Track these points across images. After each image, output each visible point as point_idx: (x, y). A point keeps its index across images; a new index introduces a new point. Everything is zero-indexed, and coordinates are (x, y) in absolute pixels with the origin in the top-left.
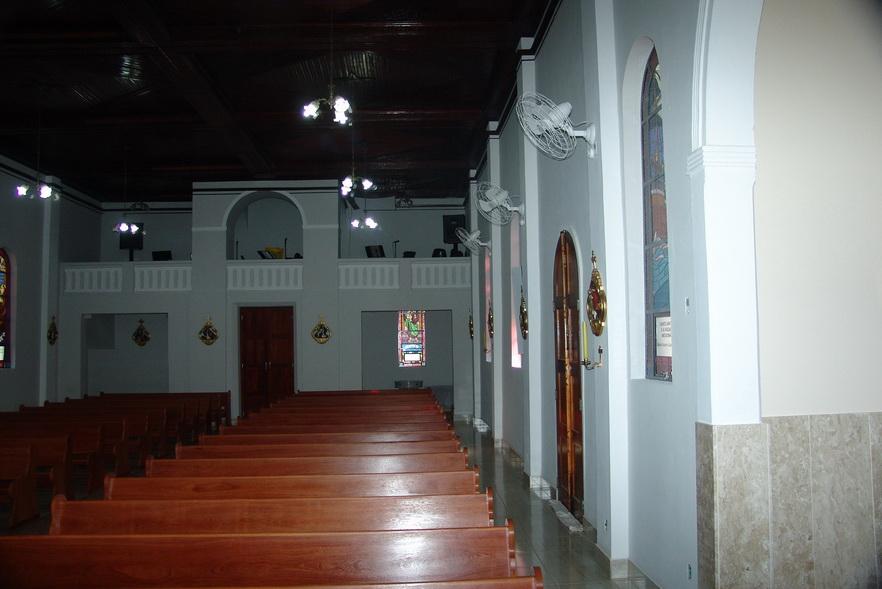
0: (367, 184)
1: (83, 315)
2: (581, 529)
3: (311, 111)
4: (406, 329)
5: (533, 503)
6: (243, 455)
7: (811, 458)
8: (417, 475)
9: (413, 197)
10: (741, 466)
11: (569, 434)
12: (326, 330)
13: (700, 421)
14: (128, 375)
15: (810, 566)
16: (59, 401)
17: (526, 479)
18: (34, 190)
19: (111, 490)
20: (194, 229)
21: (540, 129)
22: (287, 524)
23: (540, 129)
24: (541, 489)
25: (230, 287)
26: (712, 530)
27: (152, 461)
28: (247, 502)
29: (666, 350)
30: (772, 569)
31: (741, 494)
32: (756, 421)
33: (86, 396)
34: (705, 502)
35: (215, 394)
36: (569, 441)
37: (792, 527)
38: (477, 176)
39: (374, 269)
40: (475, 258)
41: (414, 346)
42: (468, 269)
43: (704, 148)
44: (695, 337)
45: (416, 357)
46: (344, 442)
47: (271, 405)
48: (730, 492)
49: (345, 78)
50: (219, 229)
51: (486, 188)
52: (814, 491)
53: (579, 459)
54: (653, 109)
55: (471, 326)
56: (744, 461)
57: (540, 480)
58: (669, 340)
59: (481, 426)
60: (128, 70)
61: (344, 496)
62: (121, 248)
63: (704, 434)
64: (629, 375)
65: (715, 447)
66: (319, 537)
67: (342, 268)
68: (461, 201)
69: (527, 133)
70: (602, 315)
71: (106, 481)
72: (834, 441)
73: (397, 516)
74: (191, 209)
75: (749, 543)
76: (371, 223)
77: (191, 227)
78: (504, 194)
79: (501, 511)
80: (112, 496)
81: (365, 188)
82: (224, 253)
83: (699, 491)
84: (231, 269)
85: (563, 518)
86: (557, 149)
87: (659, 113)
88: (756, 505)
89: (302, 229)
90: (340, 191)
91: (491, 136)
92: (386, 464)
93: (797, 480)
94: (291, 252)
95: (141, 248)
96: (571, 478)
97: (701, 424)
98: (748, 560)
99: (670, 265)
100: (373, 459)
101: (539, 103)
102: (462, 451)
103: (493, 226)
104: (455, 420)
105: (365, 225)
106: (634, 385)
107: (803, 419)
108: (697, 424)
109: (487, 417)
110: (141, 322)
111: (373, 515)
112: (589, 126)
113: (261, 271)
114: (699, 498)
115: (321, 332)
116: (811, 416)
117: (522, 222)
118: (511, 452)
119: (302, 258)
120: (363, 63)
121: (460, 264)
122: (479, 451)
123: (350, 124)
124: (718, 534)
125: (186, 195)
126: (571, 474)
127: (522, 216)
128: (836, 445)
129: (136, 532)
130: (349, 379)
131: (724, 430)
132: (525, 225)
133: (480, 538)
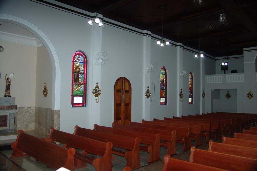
1: (212, 90)
18: (199, 56)
19: (224, 140)
20: (244, 63)
27: (236, 133)
33: (213, 112)
35: (253, 114)
60: (222, 18)
71: (223, 138)
74: (243, 57)
80: (225, 143)
95: (228, 70)
110: (228, 91)
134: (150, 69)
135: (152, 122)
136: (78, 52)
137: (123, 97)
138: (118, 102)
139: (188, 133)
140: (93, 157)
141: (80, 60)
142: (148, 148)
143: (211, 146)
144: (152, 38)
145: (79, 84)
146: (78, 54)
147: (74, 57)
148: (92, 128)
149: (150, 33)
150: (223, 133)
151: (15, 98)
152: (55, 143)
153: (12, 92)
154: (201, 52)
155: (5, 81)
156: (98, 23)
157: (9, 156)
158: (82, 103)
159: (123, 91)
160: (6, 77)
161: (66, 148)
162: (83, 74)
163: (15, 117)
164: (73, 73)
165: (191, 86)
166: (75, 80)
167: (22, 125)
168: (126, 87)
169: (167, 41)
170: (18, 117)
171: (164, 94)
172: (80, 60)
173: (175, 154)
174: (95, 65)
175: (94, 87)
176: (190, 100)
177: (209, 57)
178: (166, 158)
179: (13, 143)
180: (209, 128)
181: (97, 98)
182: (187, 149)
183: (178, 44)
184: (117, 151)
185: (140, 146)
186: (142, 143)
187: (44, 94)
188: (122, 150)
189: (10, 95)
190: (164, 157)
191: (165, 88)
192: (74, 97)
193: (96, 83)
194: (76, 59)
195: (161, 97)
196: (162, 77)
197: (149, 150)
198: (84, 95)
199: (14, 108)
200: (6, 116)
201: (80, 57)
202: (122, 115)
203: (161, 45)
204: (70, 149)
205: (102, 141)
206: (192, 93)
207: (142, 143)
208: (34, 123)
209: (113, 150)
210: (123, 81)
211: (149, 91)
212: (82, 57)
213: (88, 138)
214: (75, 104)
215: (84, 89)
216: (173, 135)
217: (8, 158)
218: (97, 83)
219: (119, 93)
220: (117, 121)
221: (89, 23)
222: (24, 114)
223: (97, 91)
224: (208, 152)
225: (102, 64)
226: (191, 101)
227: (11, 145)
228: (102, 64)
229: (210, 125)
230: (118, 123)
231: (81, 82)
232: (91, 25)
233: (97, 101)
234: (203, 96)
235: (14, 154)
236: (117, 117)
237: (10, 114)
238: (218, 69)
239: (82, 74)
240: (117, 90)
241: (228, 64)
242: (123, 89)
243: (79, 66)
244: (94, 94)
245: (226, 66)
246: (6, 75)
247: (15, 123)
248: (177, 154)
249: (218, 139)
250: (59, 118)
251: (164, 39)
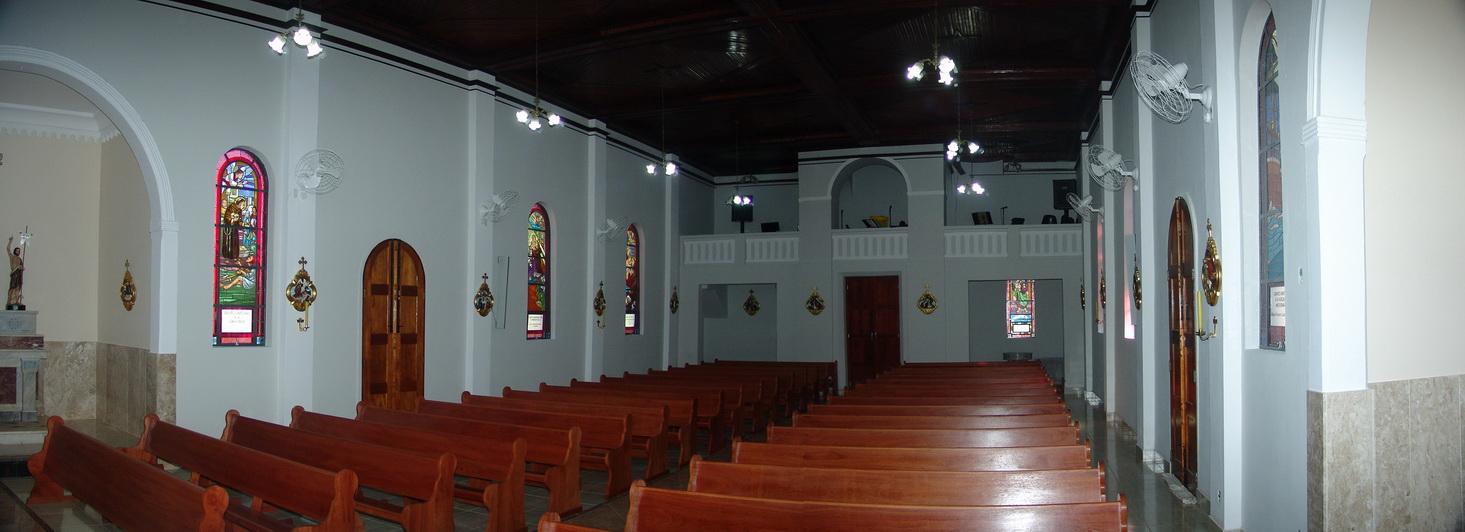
0: (974, 148)
1: (700, 286)
2: (1194, 502)
3: (915, 72)
4: (1015, 299)
5: (1146, 477)
6: (851, 425)
7: (1410, 420)
8: (1026, 450)
9: (1021, 161)
10: (1348, 431)
11: (1183, 406)
12: (931, 300)
13: (1311, 389)
14: (737, 342)
15: (1408, 519)
16: (679, 366)
17: (1139, 453)
18: (661, 168)
19: (737, 453)
21: (1155, 90)
22: (894, 496)
23: (1155, 90)
24: (1154, 462)
25: (836, 257)
26: (1321, 496)
28: (854, 472)
29: (1279, 320)
30: (1374, 525)
31: (1349, 458)
32: (1363, 387)
33: (703, 362)
34: (1315, 468)
36: (1183, 413)
37: (1393, 485)
38: (1089, 137)
39: (981, 236)
40: (1087, 225)
41: (1022, 316)
42: (1079, 239)
43: (1319, 119)
44: (1308, 307)
45: (1026, 328)
46: (947, 415)
47: (877, 376)
48: (1338, 458)
49: (950, 36)
50: (824, 198)
51: (1099, 151)
52: (1413, 450)
53: (1193, 431)
54: (1270, 76)
55: (1083, 296)
56: (1350, 426)
57: (1153, 453)
58: (1282, 310)
59: (1092, 400)
60: (736, 45)
61: (950, 470)
62: (733, 220)
63: (1315, 402)
64: (1243, 345)
65: (1325, 414)
66: (927, 511)
67: (948, 235)
68: (1072, 165)
69: (1142, 94)
70: (1217, 284)
71: (734, 445)
72: (1429, 403)
73: (1006, 491)
74: (797, 180)
75: (1354, 504)
76: (978, 189)
78: (1118, 158)
79: (1113, 485)
80: (739, 460)
81: (972, 152)
82: (828, 221)
83: (1309, 458)
84: (836, 238)
85: (1177, 491)
86: (1173, 112)
87: (1276, 80)
88: (1362, 467)
89: (906, 196)
90: (946, 156)
91: (1104, 97)
92: (994, 438)
93: (1398, 441)
94: (896, 219)
96: (1185, 450)
97: (1312, 392)
98: (1354, 521)
99: (1284, 234)
100: (981, 432)
101: (1154, 63)
102: (1073, 424)
103: (1106, 192)
104: (1066, 393)
105: (971, 190)
106: (1248, 355)
107: (1404, 383)
108: (1308, 392)
109: (1100, 389)
110: (752, 292)
111: (981, 490)
112: (1205, 89)
113: (875, 240)
114: (1309, 464)
115: (927, 302)
116: (1411, 381)
117: (1136, 188)
118: (1124, 425)
119: (907, 226)
120: (969, 20)
122: (1091, 425)
123: (956, 85)
124: (1326, 499)
125: (790, 165)
126: (1185, 447)
127: (1135, 181)
128: (1431, 406)
129: (763, 497)
130: (956, 352)
131: (1333, 398)
132: (1139, 191)
133: (1092, 514)
134: (493, 209)
135: (497, 398)
136: (237, 154)
137: (395, 310)
138: (376, 328)
139: (623, 436)
140: (290, 521)
141: (242, 181)
142: (483, 491)
143: (697, 474)
144: (497, 97)
145: (237, 266)
146: (236, 160)
147: (223, 171)
148: (286, 420)
149: (490, 79)
150: (733, 430)
151: (35, 313)
152: (162, 466)
153: (28, 294)
154: (669, 156)
155: (8, 259)
156: (305, 47)
157: (24, 497)
158: (250, 331)
159: (395, 291)
160: (9, 245)
161: (197, 486)
162: (254, 229)
163: (37, 373)
164: (218, 225)
165: (632, 272)
166: (226, 252)
167: (60, 402)
168: (406, 273)
169: (551, 112)
170: (47, 375)
171: (538, 301)
172: (242, 181)
173: (579, 510)
174: (296, 196)
175: (293, 277)
176: (630, 321)
177: (692, 174)
178: (546, 525)
179: (33, 457)
180: (691, 416)
181: (302, 315)
182: (620, 491)
183: (592, 123)
184: (373, 503)
185: (457, 486)
186: (463, 476)
187: (124, 300)
188: (392, 500)
189: (23, 303)
190: (540, 524)
191: (543, 279)
192: (223, 311)
193: (300, 262)
194: (229, 177)
195: (529, 313)
196: (533, 240)
197: (488, 499)
198: (257, 305)
199: (36, 345)
200: (13, 370)
201: (243, 169)
202: (392, 375)
203: (530, 126)
204: (210, 490)
205: (323, 467)
206: (635, 296)
207: (463, 476)
208: (95, 396)
209: (359, 497)
210: (396, 253)
211: (488, 290)
212: (249, 171)
213: (271, 453)
214: (227, 335)
215: (257, 282)
216: (571, 445)
217: (19, 502)
218: (303, 262)
219: (382, 297)
220: (375, 396)
221: (275, 48)
222: (64, 365)
223: (303, 289)
224: (687, 496)
225: (319, 193)
226: (632, 325)
227: (26, 463)
228: (319, 193)
229: (695, 405)
230: (378, 404)
231: (247, 258)
232: (281, 54)
233: (303, 325)
234: (674, 307)
235: (35, 492)
236: (373, 383)
237: (24, 364)
238: (721, 216)
239: (251, 229)
240: (374, 287)
241: (751, 201)
242: (395, 282)
243: (238, 203)
244: (290, 299)
245: (748, 208)
246: (11, 239)
247: (40, 393)
248: (584, 509)
249: (718, 449)
250: (173, 381)
251: (543, 104)
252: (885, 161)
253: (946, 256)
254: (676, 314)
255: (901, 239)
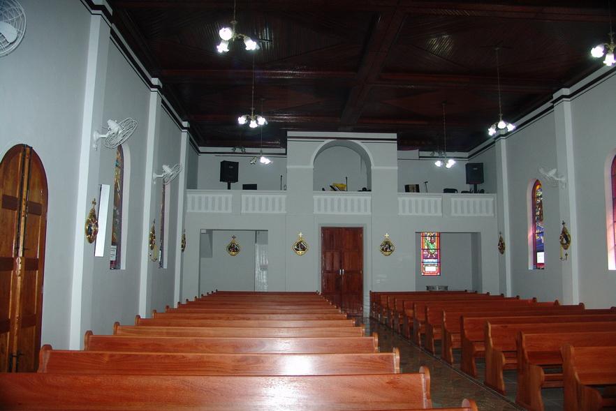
55: (183, 247)
77: (286, 165)
84: (316, 197)
92: (283, 345)
110: (234, 237)
121: (251, 196)
252: (354, 143)
253: (314, 213)
254: (503, 255)
255: (227, 199)
